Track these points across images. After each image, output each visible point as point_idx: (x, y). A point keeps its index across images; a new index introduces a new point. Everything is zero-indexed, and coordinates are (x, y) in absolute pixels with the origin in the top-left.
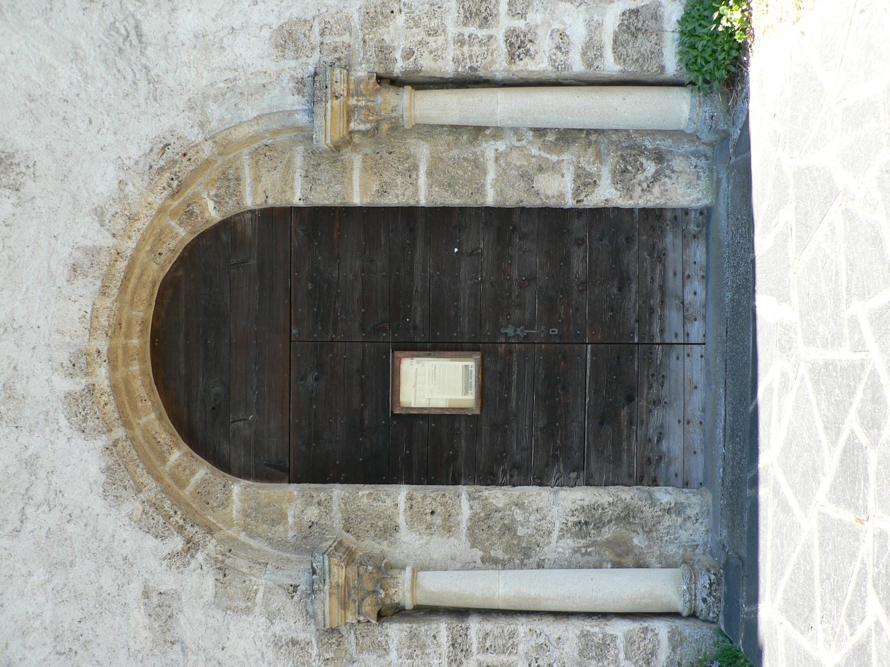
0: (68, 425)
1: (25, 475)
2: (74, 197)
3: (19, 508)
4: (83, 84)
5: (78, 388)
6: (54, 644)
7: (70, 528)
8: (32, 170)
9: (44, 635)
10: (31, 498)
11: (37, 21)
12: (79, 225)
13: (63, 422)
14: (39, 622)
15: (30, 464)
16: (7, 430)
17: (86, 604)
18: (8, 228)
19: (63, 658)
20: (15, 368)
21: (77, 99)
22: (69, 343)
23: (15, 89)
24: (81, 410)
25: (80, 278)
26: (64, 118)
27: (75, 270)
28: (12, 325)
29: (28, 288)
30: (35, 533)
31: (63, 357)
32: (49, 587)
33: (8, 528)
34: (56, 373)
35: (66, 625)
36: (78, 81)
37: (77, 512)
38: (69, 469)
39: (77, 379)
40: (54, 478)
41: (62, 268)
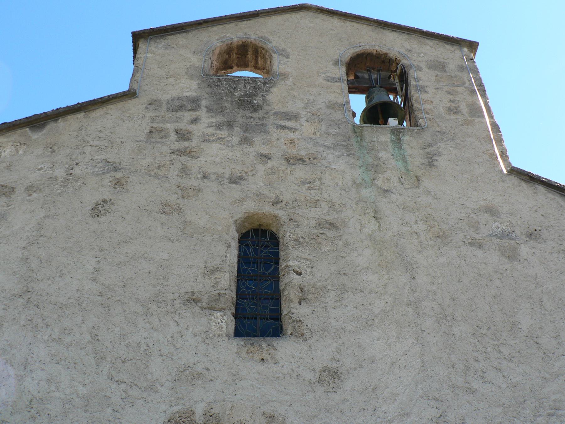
0: (174, 412)
1: (145, 384)
2: (316, 416)
3: (126, 380)
4: (385, 420)
5: (197, 418)
6: (38, 398)
7: (109, 411)
8: (331, 390)
9: (45, 392)
10: (131, 387)
11: (421, 391)
12: (298, 420)
13: (176, 409)
14: (54, 389)
15: (152, 388)
16: (174, 375)
17: (59, 418)
18: (296, 377)
19: (28, 403)
20: (211, 380)
21: (377, 416)
22: (225, 413)
23: (379, 380)
24: (183, 420)
25: (266, 420)
26: (364, 409)
27: (270, 417)
28: (237, 379)
29: (260, 388)
30: (109, 389)
31: (217, 410)
32: (74, 396)
33: (114, 373)
34: (206, 405)
35: (48, 406)
36: (387, 417)
37: (118, 415)
38: (147, 411)
39: (202, 418)
40: (141, 402)
41: (272, 409)
